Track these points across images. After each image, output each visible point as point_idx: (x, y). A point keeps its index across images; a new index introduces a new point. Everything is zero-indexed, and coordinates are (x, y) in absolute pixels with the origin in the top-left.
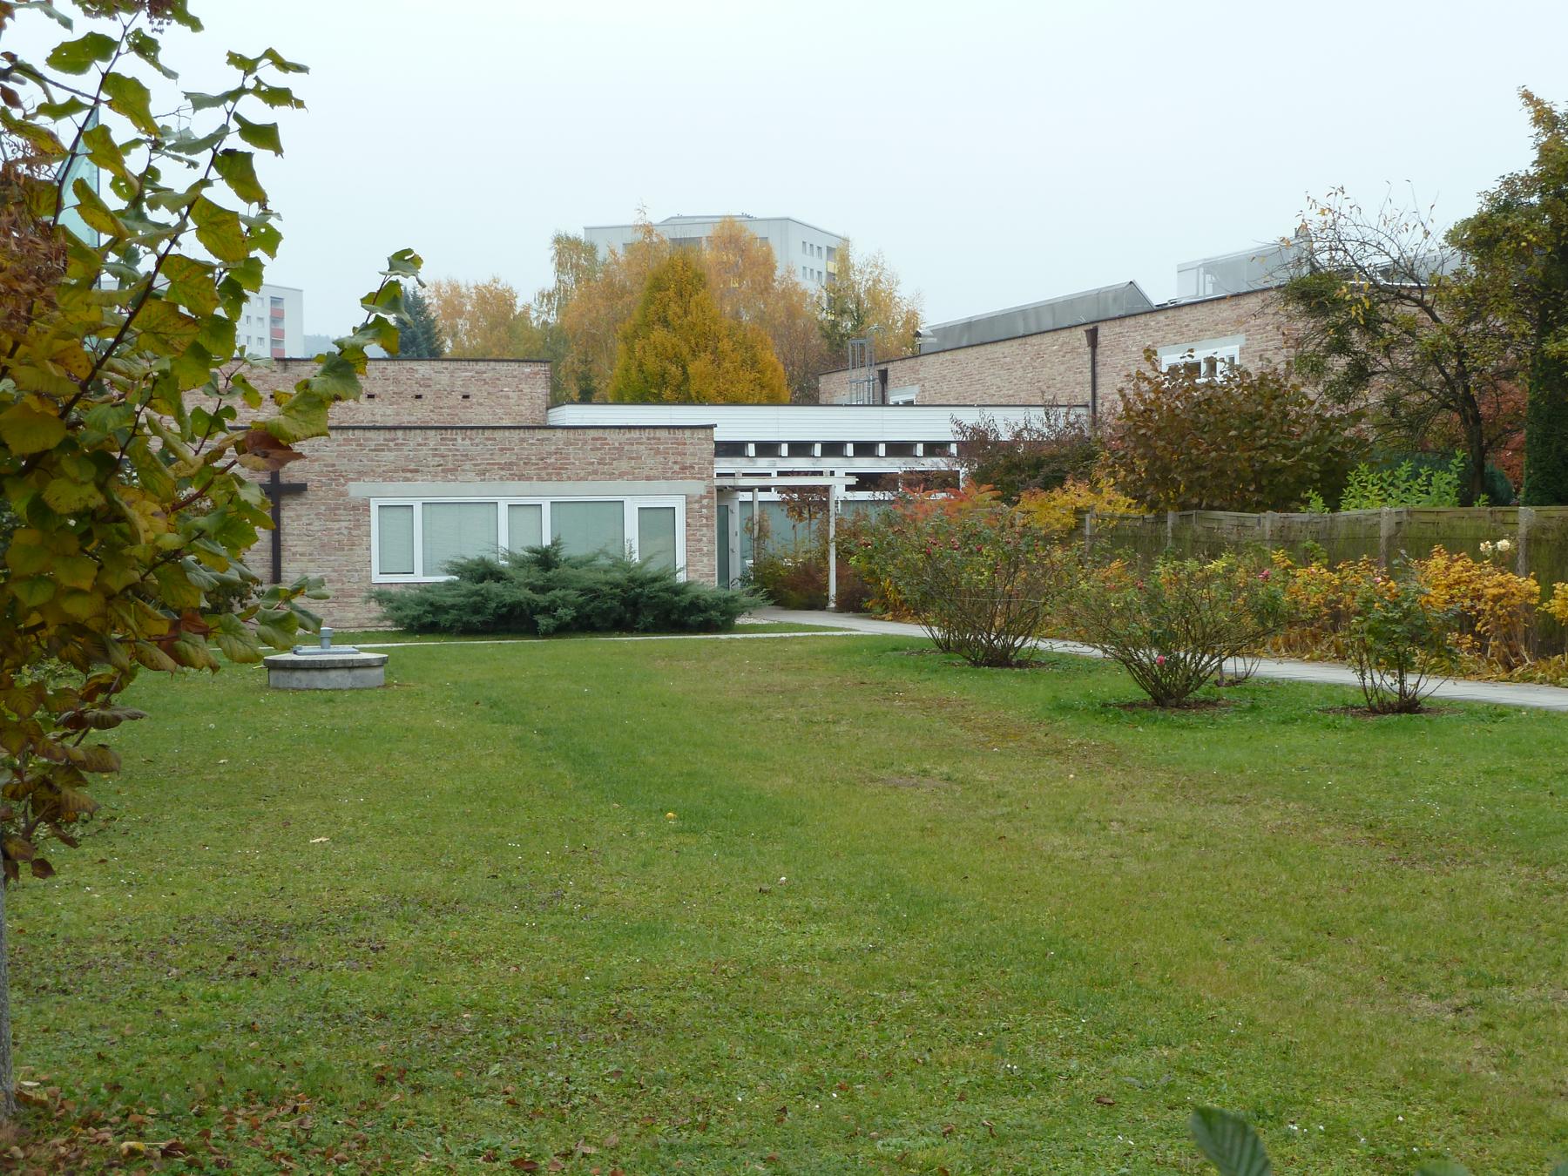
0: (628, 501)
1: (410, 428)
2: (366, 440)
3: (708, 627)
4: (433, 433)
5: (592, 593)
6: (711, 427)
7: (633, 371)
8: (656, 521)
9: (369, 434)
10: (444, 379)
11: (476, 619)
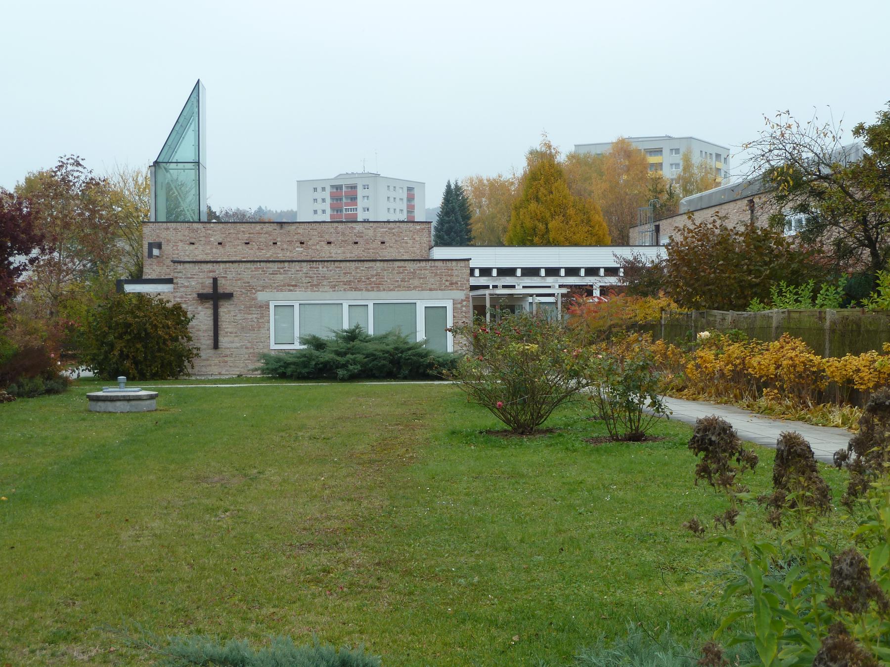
0: (418, 303)
1: (292, 261)
4: (304, 264)
5: (371, 356)
6: (468, 260)
7: (518, 227)
8: (435, 314)
9: (269, 265)
10: (371, 233)
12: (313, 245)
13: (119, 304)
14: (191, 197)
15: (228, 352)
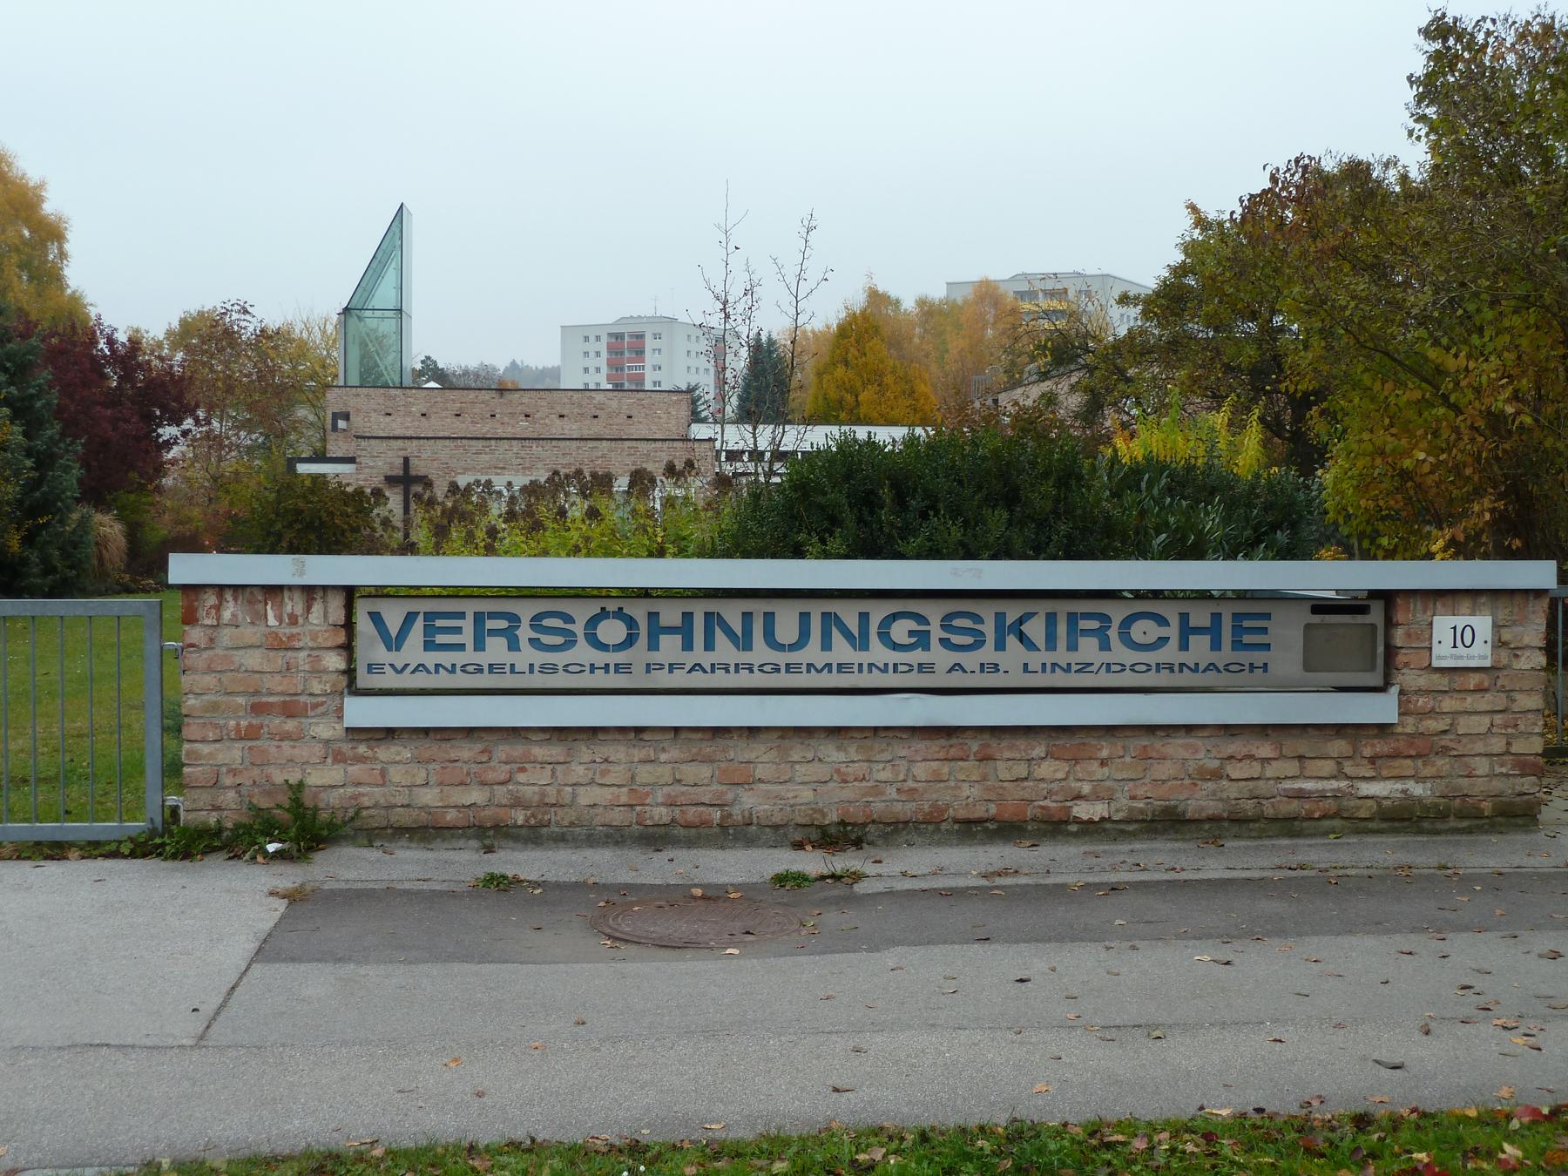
13: (289, 486)
14: (392, 357)
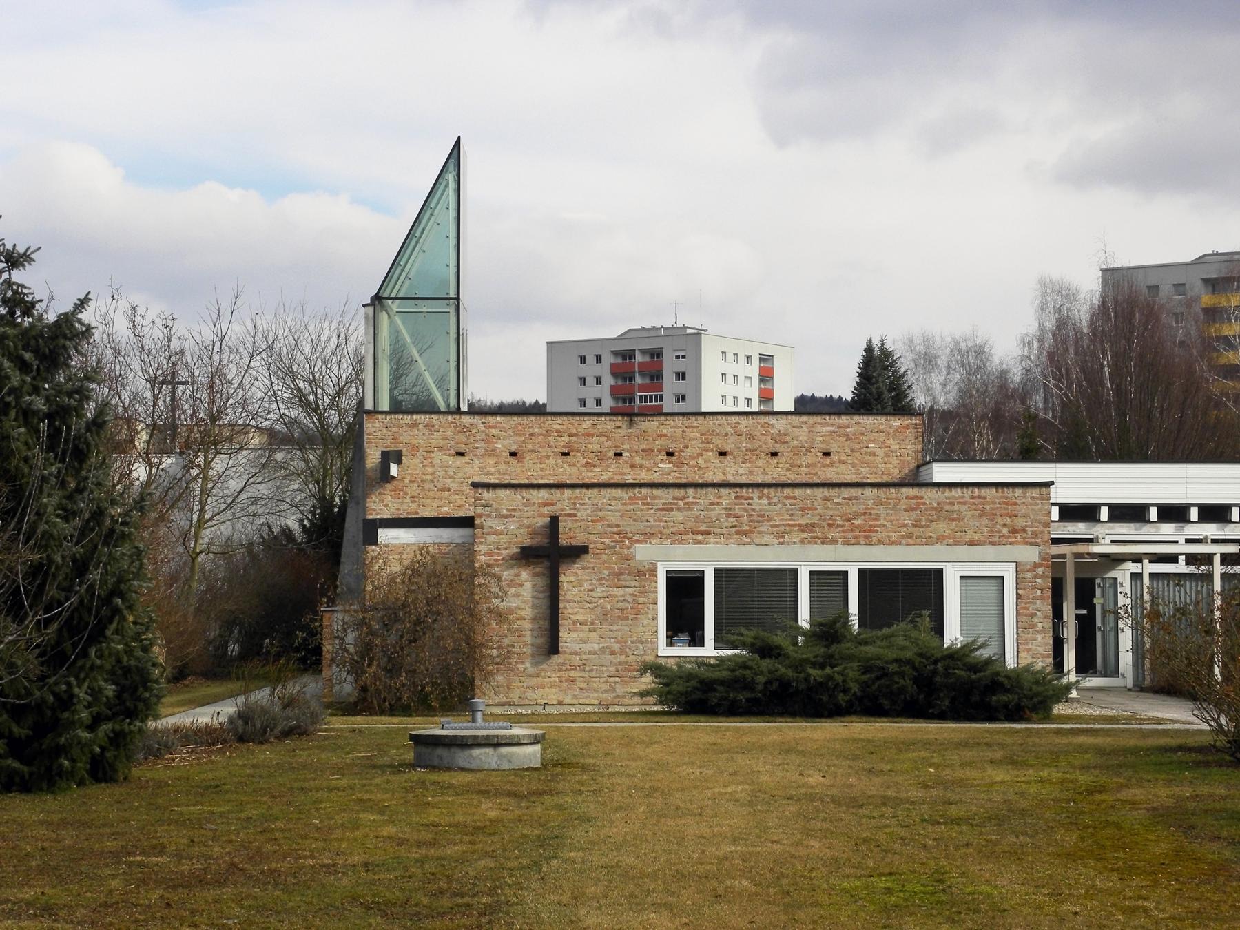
2: (654, 498)
3: (1015, 714)
9: (657, 492)
11: (742, 697)
12: (693, 458)
15: (576, 661)
